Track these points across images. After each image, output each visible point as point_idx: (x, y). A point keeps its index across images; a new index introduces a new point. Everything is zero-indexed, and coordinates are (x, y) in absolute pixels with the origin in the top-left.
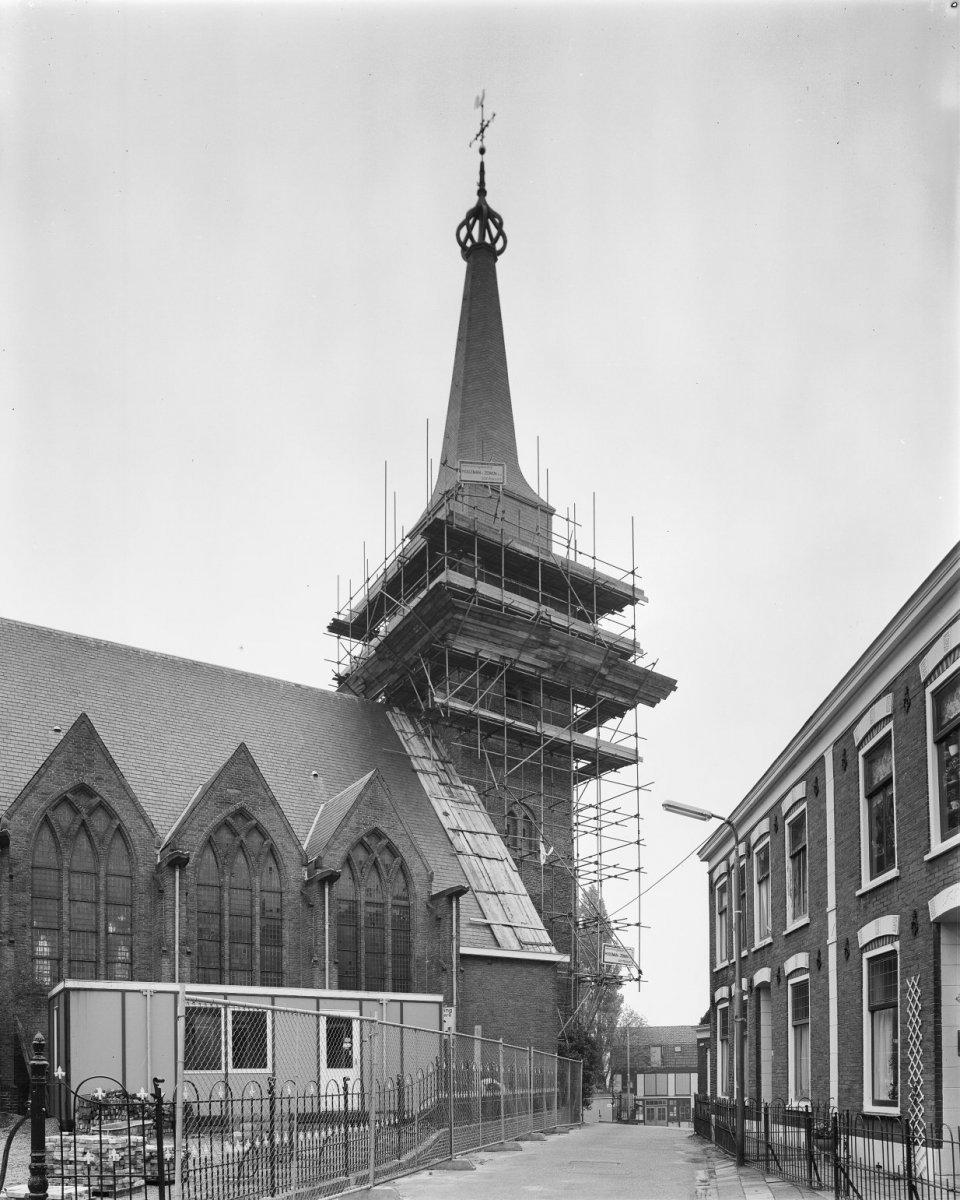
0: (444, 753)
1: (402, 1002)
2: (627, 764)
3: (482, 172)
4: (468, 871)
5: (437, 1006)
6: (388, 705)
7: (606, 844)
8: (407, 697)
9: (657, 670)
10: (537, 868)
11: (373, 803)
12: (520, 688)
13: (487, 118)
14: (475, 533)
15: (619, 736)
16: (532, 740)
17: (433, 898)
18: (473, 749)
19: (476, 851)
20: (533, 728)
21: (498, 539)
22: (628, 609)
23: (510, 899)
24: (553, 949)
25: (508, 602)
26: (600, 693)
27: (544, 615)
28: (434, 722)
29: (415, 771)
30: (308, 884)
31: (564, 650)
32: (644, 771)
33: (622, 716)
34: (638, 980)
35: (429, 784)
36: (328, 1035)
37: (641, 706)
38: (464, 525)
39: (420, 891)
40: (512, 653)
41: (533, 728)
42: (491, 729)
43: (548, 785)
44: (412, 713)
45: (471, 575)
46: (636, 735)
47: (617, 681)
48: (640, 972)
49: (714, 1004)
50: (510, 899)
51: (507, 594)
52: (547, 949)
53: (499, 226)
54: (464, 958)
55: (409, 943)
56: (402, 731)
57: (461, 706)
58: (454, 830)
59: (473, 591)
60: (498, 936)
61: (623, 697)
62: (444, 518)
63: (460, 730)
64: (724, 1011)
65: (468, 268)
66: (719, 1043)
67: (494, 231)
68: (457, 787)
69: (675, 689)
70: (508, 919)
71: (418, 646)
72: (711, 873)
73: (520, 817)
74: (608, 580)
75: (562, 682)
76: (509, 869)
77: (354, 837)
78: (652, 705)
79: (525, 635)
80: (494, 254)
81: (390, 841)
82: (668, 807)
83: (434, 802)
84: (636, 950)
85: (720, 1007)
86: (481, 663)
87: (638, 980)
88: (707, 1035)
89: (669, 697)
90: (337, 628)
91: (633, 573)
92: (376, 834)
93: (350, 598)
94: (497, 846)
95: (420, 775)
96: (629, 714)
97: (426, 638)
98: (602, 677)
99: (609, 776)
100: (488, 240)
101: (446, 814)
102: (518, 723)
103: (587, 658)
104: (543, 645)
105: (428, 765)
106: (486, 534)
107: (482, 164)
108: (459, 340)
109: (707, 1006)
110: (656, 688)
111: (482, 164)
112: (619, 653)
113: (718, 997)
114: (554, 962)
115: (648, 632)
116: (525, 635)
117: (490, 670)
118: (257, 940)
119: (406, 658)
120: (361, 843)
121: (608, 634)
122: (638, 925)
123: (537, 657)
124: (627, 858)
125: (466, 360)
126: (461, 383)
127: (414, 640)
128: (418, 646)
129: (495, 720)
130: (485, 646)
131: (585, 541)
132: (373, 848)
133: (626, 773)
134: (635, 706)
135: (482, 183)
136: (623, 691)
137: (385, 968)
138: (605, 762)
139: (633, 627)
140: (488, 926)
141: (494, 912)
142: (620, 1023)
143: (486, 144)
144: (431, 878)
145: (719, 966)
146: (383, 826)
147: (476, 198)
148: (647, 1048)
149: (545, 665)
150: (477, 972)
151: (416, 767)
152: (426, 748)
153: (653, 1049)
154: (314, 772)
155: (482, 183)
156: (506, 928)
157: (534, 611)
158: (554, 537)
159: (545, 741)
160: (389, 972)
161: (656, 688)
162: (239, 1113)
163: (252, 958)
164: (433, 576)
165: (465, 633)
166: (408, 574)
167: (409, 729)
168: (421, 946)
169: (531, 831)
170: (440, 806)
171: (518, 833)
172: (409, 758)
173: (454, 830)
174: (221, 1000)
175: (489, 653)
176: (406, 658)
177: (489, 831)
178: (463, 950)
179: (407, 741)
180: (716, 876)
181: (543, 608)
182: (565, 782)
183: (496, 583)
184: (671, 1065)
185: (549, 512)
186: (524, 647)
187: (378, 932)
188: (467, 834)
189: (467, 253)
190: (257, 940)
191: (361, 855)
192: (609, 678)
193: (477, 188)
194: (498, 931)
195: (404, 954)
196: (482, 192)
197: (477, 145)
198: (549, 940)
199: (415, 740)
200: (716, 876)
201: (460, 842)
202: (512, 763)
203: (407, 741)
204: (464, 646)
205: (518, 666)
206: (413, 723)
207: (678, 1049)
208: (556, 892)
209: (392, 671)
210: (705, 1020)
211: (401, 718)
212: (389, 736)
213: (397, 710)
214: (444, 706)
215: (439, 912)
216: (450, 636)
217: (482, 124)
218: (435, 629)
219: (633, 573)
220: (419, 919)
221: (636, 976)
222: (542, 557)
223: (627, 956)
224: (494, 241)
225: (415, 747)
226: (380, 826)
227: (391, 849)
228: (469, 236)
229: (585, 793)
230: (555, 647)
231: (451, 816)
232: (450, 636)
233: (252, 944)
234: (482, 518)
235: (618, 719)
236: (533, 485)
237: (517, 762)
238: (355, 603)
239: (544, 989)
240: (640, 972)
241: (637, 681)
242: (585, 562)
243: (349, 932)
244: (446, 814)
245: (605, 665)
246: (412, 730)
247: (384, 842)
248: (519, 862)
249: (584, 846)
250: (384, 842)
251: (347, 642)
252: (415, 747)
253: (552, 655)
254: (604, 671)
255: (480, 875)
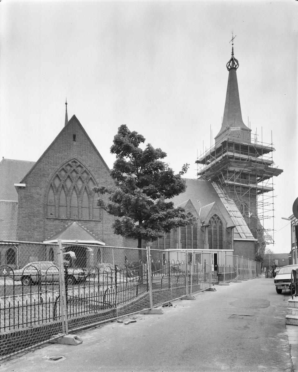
0: (225, 192)
1: (226, 251)
2: (270, 191)
3: (233, 49)
4: (233, 221)
5: (232, 252)
6: (211, 181)
7: (264, 211)
8: (217, 178)
9: (278, 168)
10: (248, 217)
11: (215, 209)
12: (244, 176)
13: (234, 36)
14: (234, 142)
15: (267, 184)
16: (248, 188)
17: (227, 228)
18: (231, 191)
19: (235, 216)
20: (247, 185)
21: (239, 143)
22: (270, 153)
23: (243, 227)
24: (254, 238)
25: (242, 157)
26: (264, 175)
27: (250, 158)
28: (223, 186)
29: (219, 197)
30: (202, 227)
31: (255, 167)
32: (275, 192)
33: (269, 179)
34: (273, 243)
35: (223, 200)
36: (14, 259)
37: (274, 176)
38: (231, 141)
39: (224, 227)
40: (242, 169)
41: (247, 185)
42: (238, 186)
43: (251, 197)
44: (218, 183)
45: (233, 152)
46: (273, 184)
47: (268, 172)
48: (274, 241)
49: (292, 250)
50: (243, 227)
51: (241, 155)
52: (252, 238)
53: (237, 62)
54: (235, 241)
55: (222, 238)
56: (215, 187)
57: (231, 182)
58: (229, 211)
59: (233, 156)
60: (241, 235)
61: (269, 175)
62: (227, 140)
63: (230, 187)
64: (294, 252)
65: (230, 74)
66: (293, 258)
67: (236, 63)
68: (229, 200)
69: (283, 172)
70: (244, 232)
71: (220, 169)
72: (291, 222)
73: (244, 205)
74: (266, 147)
75: (254, 173)
76: (242, 219)
77: (211, 217)
78: (277, 176)
79: (246, 165)
80: (235, 69)
81: (218, 217)
82: (282, 218)
83: (224, 204)
84: (273, 236)
85: (293, 251)
86: (235, 172)
87: (273, 243)
88: (291, 257)
89: (281, 174)
90: (198, 162)
91: (272, 144)
92: (215, 215)
93: (202, 155)
94: (239, 214)
95: (220, 198)
96: (271, 179)
97: (222, 168)
98: (264, 171)
99: (265, 194)
100: (234, 66)
101: (227, 207)
102: (244, 185)
103: (260, 168)
104: (250, 166)
105: (222, 195)
106: (236, 142)
107: (233, 48)
108: (227, 91)
109: (291, 250)
110: (277, 172)
111: (233, 48)
112: (267, 164)
113: (293, 249)
114: (254, 241)
115: (276, 159)
116: (246, 165)
117: (237, 173)
118: (192, 239)
119: (217, 171)
120: (212, 217)
121: (266, 160)
122: (273, 230)
123: (248, 169)
124: (270, 214)
125: (229, 97)
126: (228, 102)
127: (220, 168)
128: (220, 169)
129: (238, 185)
130: (236, 168)
131: (259, 138)
132: (216, 219)
133: (270, 193)
134: (272, 177)
135: (233, 52)
136: (269, 174)
137: (217, 243)
138: (263, 191)
139: (272, 157)
140: (239, 233)
141: (240, 231)
142: (266, 252)
143: (234, 43)
144: (227, 224)
145: (293, 242)
146: (217, 214)
147: (231, 56)
148: (274, 260)
149: (250, 170)
150: (237, 244)
151: (220, 196)
152: (221, 191)
153: (276, 260)
154: (198, 200)
155: (233, 52)
156: (243, 234)
157: (247, 158)
158: (251, 139)
159: (250, 188)
160: (218, 244)
161: (277, 172)
162: (34, 301)
163: (191, 243)
164: (224, 153)
165: (232, 166)
166: (217, 152)
167: (217, 187)
168: (225, 238)
169: (246, 209)
170: (226, 205)
171: (244, 210)
172: (217, 194)
173: (229, 211)
174: (201, 252)
175: (237, 169)
176: (217, 171)
177: (237, 210)
178: (234, 239)
179: (217, 190)
180: (292, 223)
181: (250, 156)
182: (254, 197)
183: (239, 153)
184: (281, 264)
185: (250, 131)
186: (245, 167)
187: (216, 236)
188: (232, 212)
189: (229, 70)
190: (192, 239)
191: (212, 220)
192: (266, 171)
193: (232, 54)
194: (241, 235)
195: (221, 240)
196: (233, 54)
197: (232, 43)
198: (252, 236)
199: (219, 190)
200: (292, 223)
201: (231, 214)
202: (242, 194)
203: (217, 190)
204: (231, 169)
205: (244, 171)
206: (218, 185)
207: (283, 260)
208: (254, 225)
209: (213, 174)
210: (290, 253)
211: (215, 184)
212: (212, 189)
213: (213, 182)
214: (227, 183)
215: (229, 231)
216: (228, 167)
217: (233, 41)
218: (225, 166)
219: (272, 144)
220: (224, 233)
221: (273, 242)
222: (249, 145)
223: (270, 237)
224: (236, 66)
225: (219, 191)
226: (216, 213)
227: (219, 218)
228: (229, 65)
229: (260, 198)
230: (253, 166)
231: (228, 208)
232: (228, 167)
233: (191, 240)
234: (235, 138)
235: (268, 180)
236: (247, 126)
237: (244, 194)
238: (202, 156)
239: (252, 247)
240: (274, 241)
241: (273, 171)
242: (259, 144)
243: (210, 236)
244: (227, 207)
245: (265, 169)
246: (218, 187)
247: (217, 217)
248: (244, 216)
249: (259, 211)
250: (217, 217)
251: (200, 165)
252: (219, 191)
253: (252, 168)
254: (264, 170)
255: (236, 221)
